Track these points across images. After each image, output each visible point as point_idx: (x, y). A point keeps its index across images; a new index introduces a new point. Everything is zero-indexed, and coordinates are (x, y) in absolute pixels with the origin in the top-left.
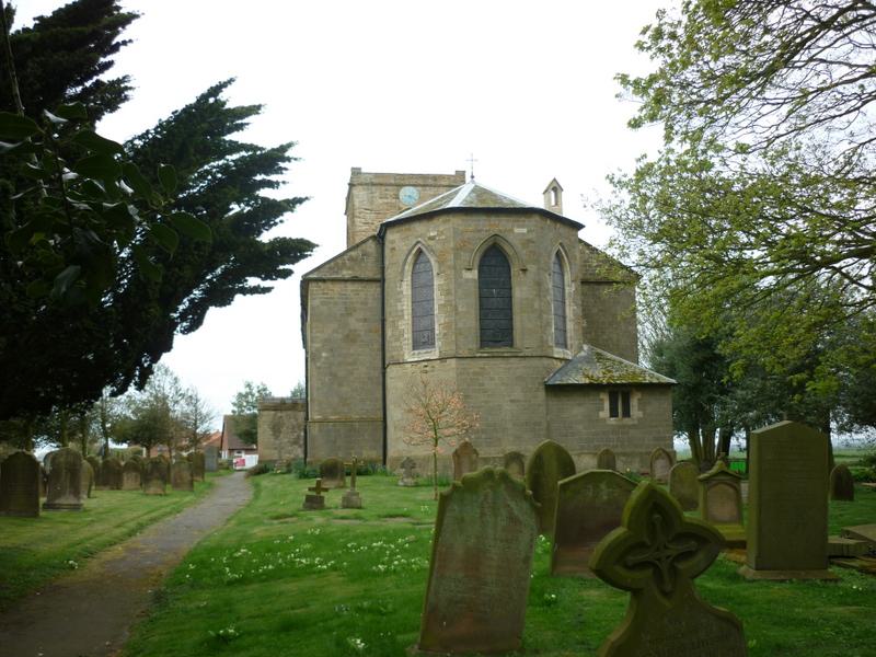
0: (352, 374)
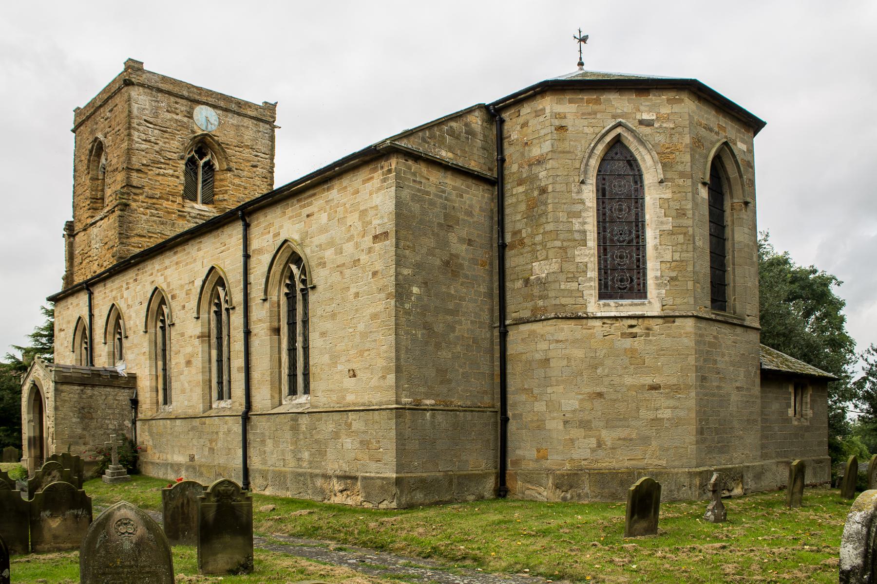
0: (453, 329)
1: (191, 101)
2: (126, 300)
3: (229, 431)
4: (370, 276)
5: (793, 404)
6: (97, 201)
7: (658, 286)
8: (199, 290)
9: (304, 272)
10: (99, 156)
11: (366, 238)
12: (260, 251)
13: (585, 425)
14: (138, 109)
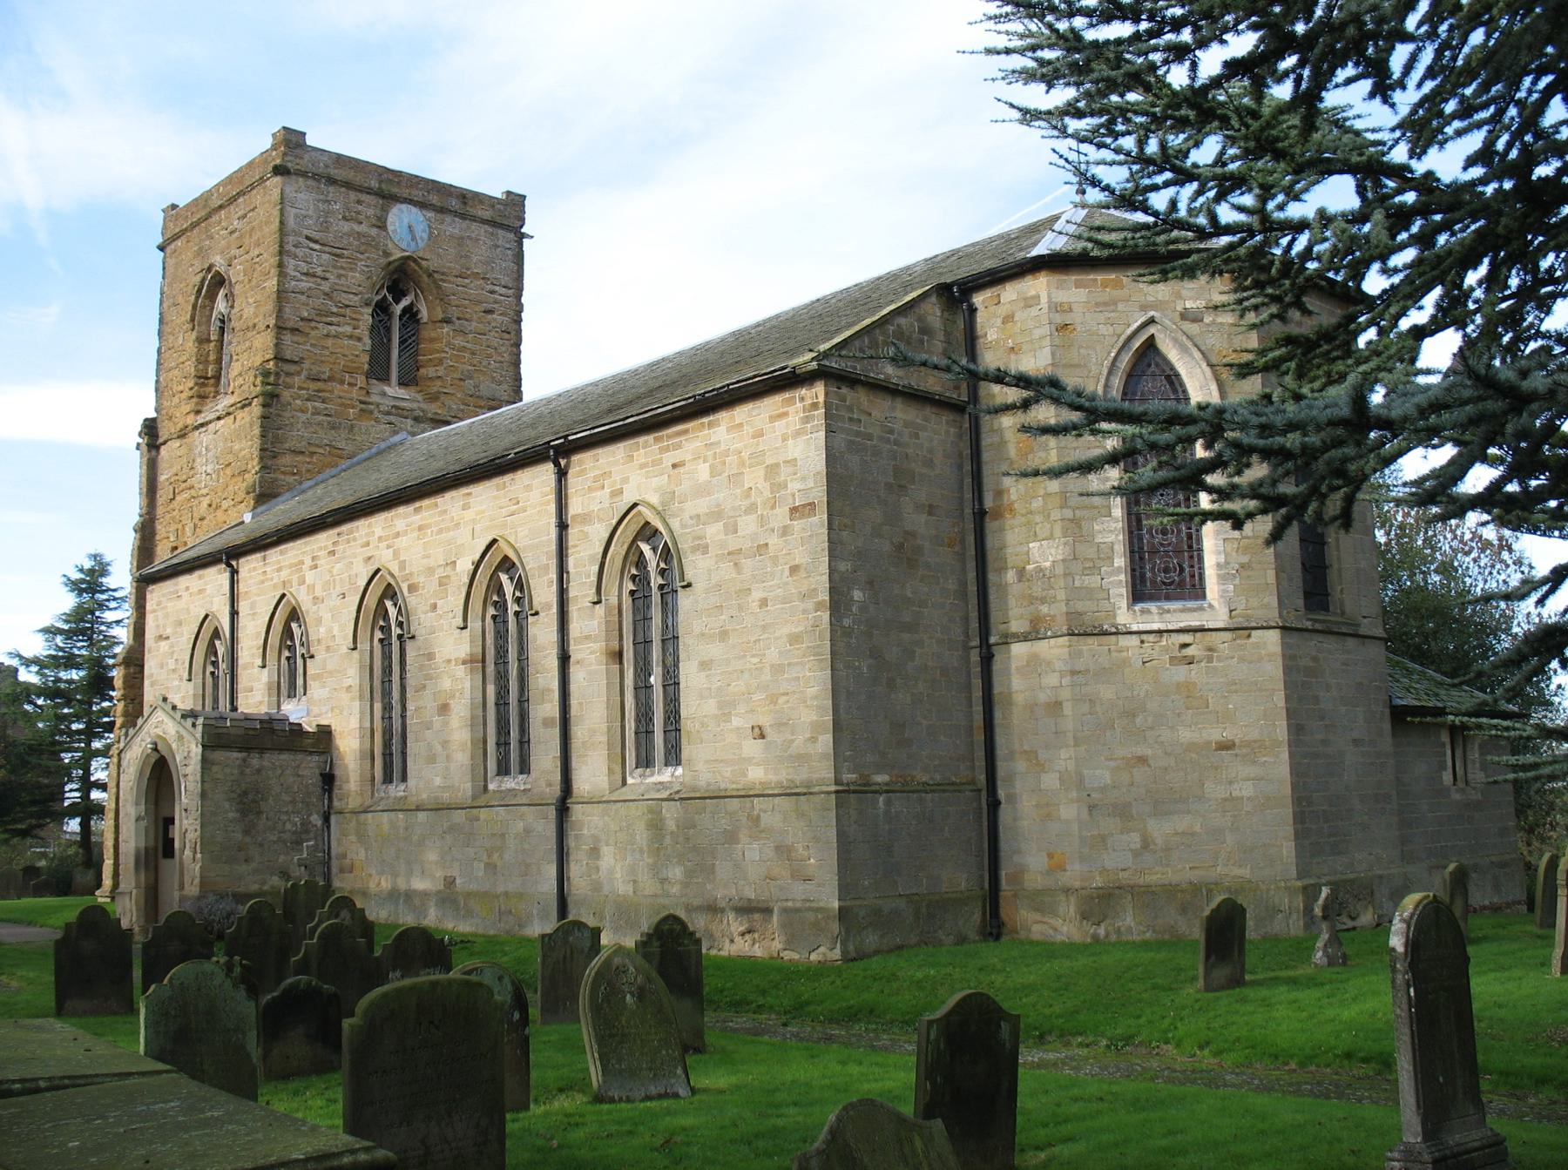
1: (383, 197)
2: (311, 588)
3: (527, 831)
4: (787, 573)
5: (1449, 763)
6: (208, 381)
7: (1223, 579)
8: (466, 580)
9: (666, 554)
10: (212, 297)
11: (778, 510)
12: (586, 518)
13: (1122, 811)
14: (296, 216)
